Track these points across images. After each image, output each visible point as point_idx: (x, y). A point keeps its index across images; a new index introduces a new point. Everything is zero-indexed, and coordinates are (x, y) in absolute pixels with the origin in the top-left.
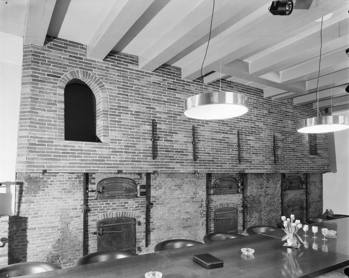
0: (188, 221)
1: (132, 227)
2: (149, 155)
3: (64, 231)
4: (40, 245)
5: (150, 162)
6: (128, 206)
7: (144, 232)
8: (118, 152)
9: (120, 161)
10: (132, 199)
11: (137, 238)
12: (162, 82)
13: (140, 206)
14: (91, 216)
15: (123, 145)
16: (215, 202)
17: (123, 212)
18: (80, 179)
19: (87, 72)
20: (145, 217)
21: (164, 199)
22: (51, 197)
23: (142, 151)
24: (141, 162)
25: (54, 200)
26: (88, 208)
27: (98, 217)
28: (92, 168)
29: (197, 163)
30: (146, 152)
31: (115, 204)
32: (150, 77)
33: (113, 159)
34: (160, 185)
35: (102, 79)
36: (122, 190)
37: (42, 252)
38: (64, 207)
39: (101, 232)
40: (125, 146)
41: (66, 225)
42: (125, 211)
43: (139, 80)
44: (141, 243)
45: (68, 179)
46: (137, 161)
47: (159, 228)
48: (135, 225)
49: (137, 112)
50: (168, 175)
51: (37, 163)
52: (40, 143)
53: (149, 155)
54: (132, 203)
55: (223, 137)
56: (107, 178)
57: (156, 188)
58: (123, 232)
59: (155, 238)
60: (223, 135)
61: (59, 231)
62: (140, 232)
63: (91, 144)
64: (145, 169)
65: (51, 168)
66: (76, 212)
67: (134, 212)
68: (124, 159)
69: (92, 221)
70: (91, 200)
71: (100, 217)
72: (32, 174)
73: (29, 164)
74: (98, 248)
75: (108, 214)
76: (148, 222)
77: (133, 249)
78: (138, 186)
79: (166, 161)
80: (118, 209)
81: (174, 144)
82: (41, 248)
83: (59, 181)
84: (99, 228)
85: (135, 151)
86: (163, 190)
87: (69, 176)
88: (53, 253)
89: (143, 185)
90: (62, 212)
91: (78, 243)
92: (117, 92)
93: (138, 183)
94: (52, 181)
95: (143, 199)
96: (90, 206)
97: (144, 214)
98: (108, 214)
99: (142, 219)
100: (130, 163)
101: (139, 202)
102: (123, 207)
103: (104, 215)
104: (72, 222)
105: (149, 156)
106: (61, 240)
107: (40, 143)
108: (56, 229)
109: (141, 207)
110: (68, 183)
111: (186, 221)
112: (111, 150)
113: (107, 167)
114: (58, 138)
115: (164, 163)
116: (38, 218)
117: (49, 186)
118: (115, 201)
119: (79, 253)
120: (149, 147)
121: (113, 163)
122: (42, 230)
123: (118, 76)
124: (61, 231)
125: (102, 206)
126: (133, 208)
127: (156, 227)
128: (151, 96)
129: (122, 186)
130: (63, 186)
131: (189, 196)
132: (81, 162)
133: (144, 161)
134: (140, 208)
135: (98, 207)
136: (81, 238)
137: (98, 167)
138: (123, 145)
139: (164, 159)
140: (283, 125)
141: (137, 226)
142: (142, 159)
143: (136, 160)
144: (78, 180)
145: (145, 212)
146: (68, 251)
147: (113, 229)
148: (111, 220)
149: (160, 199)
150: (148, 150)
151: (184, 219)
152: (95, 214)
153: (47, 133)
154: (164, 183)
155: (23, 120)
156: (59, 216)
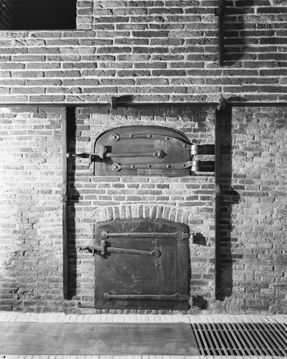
1: (179, 245)
2: (208, 53)
5: (211, 73)
6: (170, 193)
7: (211, 260)
8: (117, 50)
9: (121, 74)
10: (179, 179)
11: (193, 273)
13: (200, 195)
15: (131, 31)
17: (155, 208)
18: (57, 130)
20: (214, 224)
24: (184, 73)
25: (7, 170)
26: (75, 191)
27: (249, 274)
30: (197, 45)
31: (137, 186)
33: (101, 69)
34: (255, 145)
36: (152, 156)
39: (101, 248)
40: (134, 34)
41: (30, 224)
42: (162, 205)
44: (204, 288)
46: (169, 73)
47: (254, 255)
48: (186, 240)
50: (279, 122)
53: (208, 53)
54: (177, 186)
56: (116, 126)
57: (243, 154)
58: (157, 254)
59: (241, 279)
61: (17, 236)
62: (201, 260)
63: (46, 35)
64: (195, 94)
67: (185, 209)
68: (133, 69)
70: (80, 175)
71: (102, 215)
74: (96, 283)
77: (182, 299)
78: (193, 147)
80: (144, 198)
83: (17, 133)
84: (97, 237)
85: (165, 46)
87: (35, 122)
88: (6, 277)
89: (208, 146)
91: (54, 266)
93: (194, 141)
95: (207, 180)
96: (78, 189)
97: (212, 217)
98: (120, 209)
99: (207, 227)
100: (152, 77)
101: (198, 187)
102: (155, 196)
103: (110, 209)
104: (41, 220)
105: (208, 58)
106: (21, 254)
108: (11, 231)
109: (203, 198)
110: (34, 136)
112: (98, 47)
115: (259, 77)
118: (136, 179)
119: (56, 286)
120: (210, 33)
121: (102, 80)
124: (20, 235)
125: (106, 189)
127: (245, 253)
129: (152, 146)
130: (25, 143)
133: (191, 73)
134: (199, 200)
135: (97, 192)
138: (131, 31)
139: (257, 65)
141: (193, 246)
142: (188, 65)
143: (169, 68)
144: (53, 130)
145: (214, 213)
148: (127, 224)
149: (257, 182)
150: (205, 41)
152: (90, 206)
154: (269, 141)
156: (17, 204)
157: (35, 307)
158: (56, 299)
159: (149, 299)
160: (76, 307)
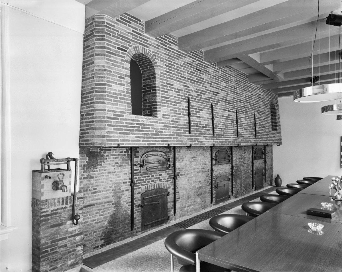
0: (200, 189)
3: (117, 205)
4: (98, 221)
10: (164, 171)
12: (192, 63)
14: (136, 189)
16: (216, 171)
19: (145, 48)
21: (186, 170)
22: (107, 171)
23: (182, 126)
27: (142, 189)
28: (152, 142)
29: (215, 137)
32: (185, 57)
35: (155, 56)
37: (100, 228)
38: (117, 182)
43: (178, 60)
45: (119, 153)
49: (179, 90)
51: (114, 137)
52: (115, 117)
55: (229, 115)
57: (179, 160)
60: (228, 113)
65: (123, 142)
66: (126, 185)
67: (166, 183)
69: (137, 194)
72: (91, 148)
73: (110, 138)
75: (149, 186)
76: (175, 193)
79: (197, 135)
80: (156, 181)
81: (201, 120)
82: (99, 224)
83: (113, 155)
86: (184, 162)
88: (109, 228)
90: (115, 187)
92: (165, 70)
94: (107, 156)
98: (149, 186)
99: (171, 191)
102: (159, 179)
104: (123, 196)
107: (115, 117)
108: (111, 204)
111: (199, 190)
113: (162, 141)
114: (127, 113)
116: (97, 194)
117: (105, 160)
119: (128, 226)
122: (100, 205)
123: (165, 54)
124: (115, 205)
125: (144, 178)
126: (165, 179)
128: (186, 75)
131: (201, 167)
132: (144, 136)
135: (142, 180)
136: (129, 212)
137: (156, 141)
140: (258, 105)
144: (127, 153)
146: (120, 225)
147: (153, 201)
151: (198, 188)
153: (119, 107)
155: (99, 92)
157: (120, 239)
158: (128, 232)
159: (158, 222)
160: (135, 233)
